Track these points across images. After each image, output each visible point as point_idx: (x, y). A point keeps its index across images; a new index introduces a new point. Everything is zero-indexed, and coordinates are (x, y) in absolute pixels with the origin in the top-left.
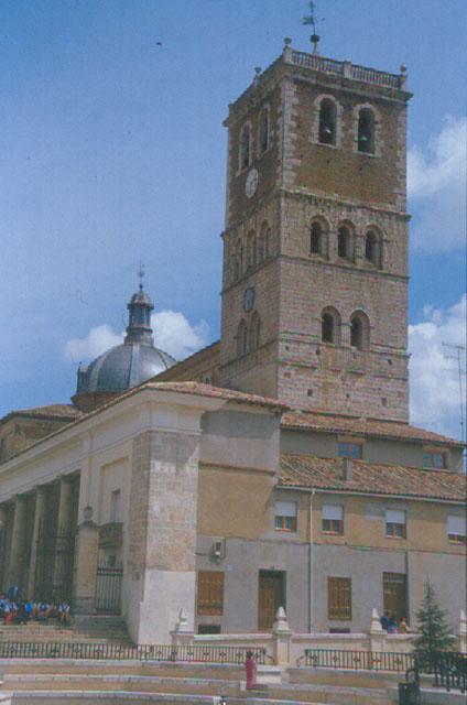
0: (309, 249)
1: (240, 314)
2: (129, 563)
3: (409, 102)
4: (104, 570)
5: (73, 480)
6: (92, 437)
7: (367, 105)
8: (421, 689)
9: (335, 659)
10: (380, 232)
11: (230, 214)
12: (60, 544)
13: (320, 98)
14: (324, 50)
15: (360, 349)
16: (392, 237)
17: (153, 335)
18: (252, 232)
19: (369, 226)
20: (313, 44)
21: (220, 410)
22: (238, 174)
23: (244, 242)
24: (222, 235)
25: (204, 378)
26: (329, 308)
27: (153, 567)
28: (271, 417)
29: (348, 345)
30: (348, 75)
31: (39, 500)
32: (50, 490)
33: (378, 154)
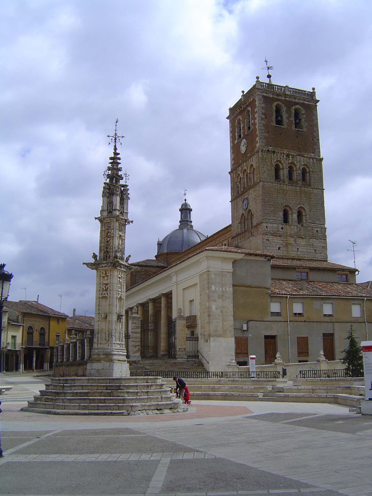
0: (274, 178)
1: (241, 212)
2: (201, 334)
3: (317, 104)
4: (189, 338)
5: (168, 296)
6: (177, 275)
7: (297, 106)
8: (190, 392)
9: (315, 374)
10: (308, 167)
11: (233, 162)
12: (151, 326)
13: (276, 103)
14: (275, 81)
15: (302, 225)
16: (315, 170)
17: (192, 224)
18: (245, 170)
19: (303, 165)
20: (269, 79)
21: (241, 259)
22: (236, 142)
23: (241, 176)
24: (229, 173)
25: (224, 243)
26: (286, 206)
27: (214, 336)
28: (266, 261)
29: (297, 224)
30: (287, 93)
31: (151, 306)
32: (156, 301)
33: (305, 129)
